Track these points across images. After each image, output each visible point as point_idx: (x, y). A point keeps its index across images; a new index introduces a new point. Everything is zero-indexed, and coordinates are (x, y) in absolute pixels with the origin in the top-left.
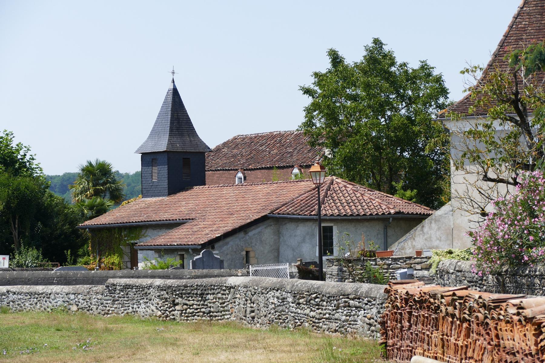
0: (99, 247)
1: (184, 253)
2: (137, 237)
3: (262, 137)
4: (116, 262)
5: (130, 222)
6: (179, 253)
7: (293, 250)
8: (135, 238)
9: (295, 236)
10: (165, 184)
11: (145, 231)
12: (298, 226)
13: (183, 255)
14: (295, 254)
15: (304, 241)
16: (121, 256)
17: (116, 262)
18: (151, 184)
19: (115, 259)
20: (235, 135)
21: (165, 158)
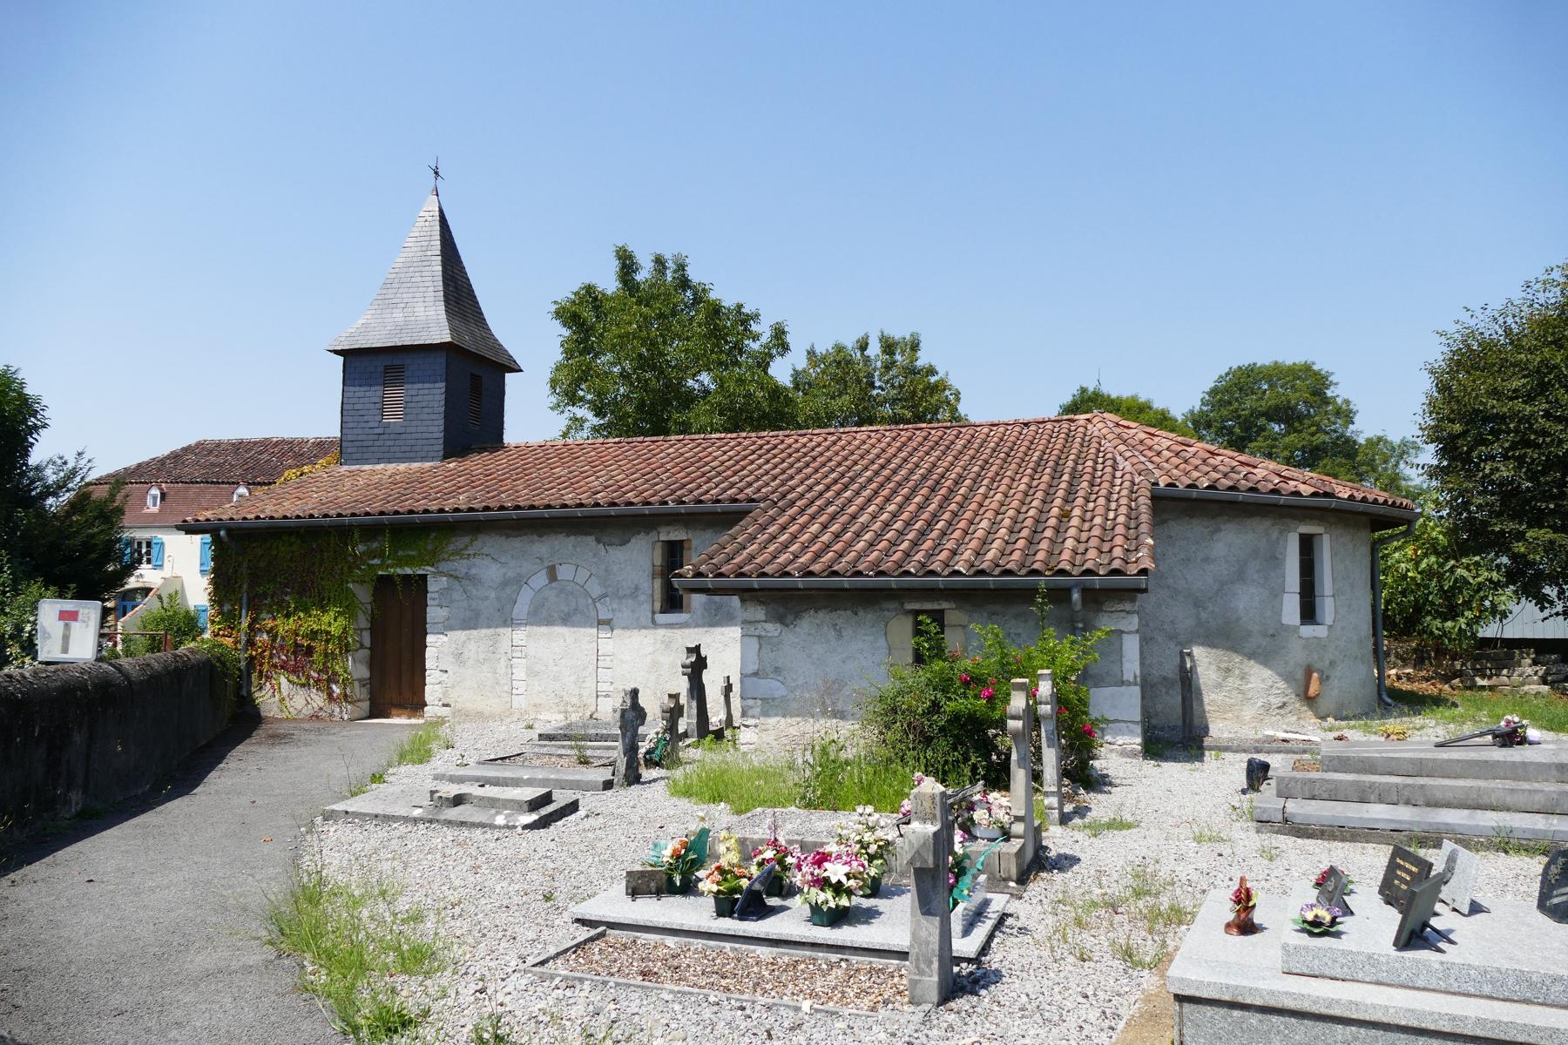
0: (251, 586)
1: (945, 605)
2: (433, 558)
3: (255, 443)
4: (335, 629)
5: (518, 507)
6: (909, 606)
7: (1198, 604)
8: (423, 562)
9: (1206, 560)
10: (435, 428)
11: (466, 539)
12: (1218, 530)
13: (942, 611)
14: (1204, 615)
15: (1240, 576)
16: (349, 611)
17: (335, 629)
18: (380, 431)
19: (331, 621)
20: (201, 438)
21: (440, 362)
